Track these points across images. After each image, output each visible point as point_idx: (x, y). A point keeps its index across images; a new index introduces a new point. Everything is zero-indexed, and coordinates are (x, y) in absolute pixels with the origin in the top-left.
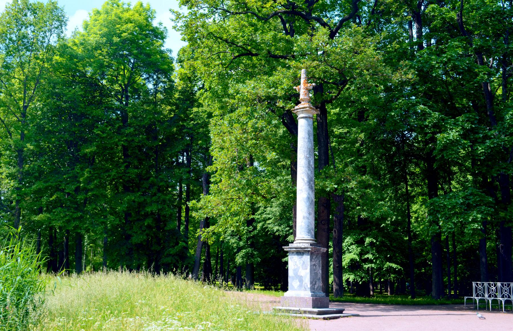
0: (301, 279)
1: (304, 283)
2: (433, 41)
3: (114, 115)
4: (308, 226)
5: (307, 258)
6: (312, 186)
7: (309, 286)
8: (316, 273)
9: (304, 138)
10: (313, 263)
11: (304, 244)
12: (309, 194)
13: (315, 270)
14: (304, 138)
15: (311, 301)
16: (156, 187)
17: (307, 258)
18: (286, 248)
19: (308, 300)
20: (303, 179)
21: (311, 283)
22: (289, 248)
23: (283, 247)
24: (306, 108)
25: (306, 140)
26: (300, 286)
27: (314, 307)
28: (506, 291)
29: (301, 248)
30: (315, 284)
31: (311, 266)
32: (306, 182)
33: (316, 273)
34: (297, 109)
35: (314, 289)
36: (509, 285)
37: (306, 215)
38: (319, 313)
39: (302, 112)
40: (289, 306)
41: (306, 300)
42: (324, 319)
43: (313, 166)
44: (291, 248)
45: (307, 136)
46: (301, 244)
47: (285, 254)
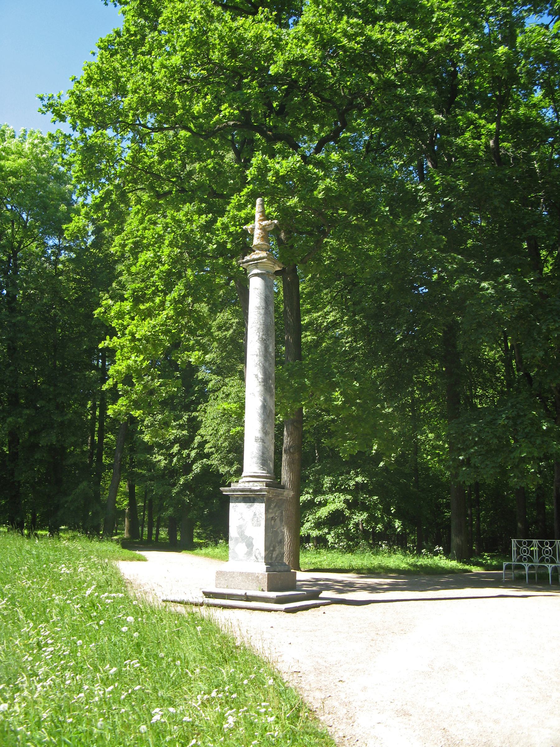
0: (250, 545)
1: (254, 549)
2: (282, 235)
3: (417, 396)
4: (263, 453)
5: (260, 508)
6: (270, 387)
7: (263, 554)
8: (276, 531)
9: (258, 308)
10: (271, 516)
11: (256, 484)
12: (265, 400)
13: (273, 527)
14: (258, 308)
15: (266, 580)
16: (272, 172)
17: (260, 508)
18: (225, 490)
19: (261, 577)
20: (256, 376)
21: (267, 548)
22: (230, 491)
23: (222, 489)
24: (263, 258)
25: (262, 311)
26: (249, 553)
27: (270, 590)
28: (547, 552)
29: (251, 491)
30: (274, 550)
31: (266, 520)
32: (260, 380)
33: (276, 531)
34: (247, 262)
35: (271, 558)
36: (552, 544)
37: (259, 434)
38: (279, 601)
39: (256, 266)
40: (227, 587)
41: (258, 577)
42: (288, 611)
43: (273, 354)
44: (234, 491)
45: (263, 304)
46: (251, 484)
47: (225, 501)
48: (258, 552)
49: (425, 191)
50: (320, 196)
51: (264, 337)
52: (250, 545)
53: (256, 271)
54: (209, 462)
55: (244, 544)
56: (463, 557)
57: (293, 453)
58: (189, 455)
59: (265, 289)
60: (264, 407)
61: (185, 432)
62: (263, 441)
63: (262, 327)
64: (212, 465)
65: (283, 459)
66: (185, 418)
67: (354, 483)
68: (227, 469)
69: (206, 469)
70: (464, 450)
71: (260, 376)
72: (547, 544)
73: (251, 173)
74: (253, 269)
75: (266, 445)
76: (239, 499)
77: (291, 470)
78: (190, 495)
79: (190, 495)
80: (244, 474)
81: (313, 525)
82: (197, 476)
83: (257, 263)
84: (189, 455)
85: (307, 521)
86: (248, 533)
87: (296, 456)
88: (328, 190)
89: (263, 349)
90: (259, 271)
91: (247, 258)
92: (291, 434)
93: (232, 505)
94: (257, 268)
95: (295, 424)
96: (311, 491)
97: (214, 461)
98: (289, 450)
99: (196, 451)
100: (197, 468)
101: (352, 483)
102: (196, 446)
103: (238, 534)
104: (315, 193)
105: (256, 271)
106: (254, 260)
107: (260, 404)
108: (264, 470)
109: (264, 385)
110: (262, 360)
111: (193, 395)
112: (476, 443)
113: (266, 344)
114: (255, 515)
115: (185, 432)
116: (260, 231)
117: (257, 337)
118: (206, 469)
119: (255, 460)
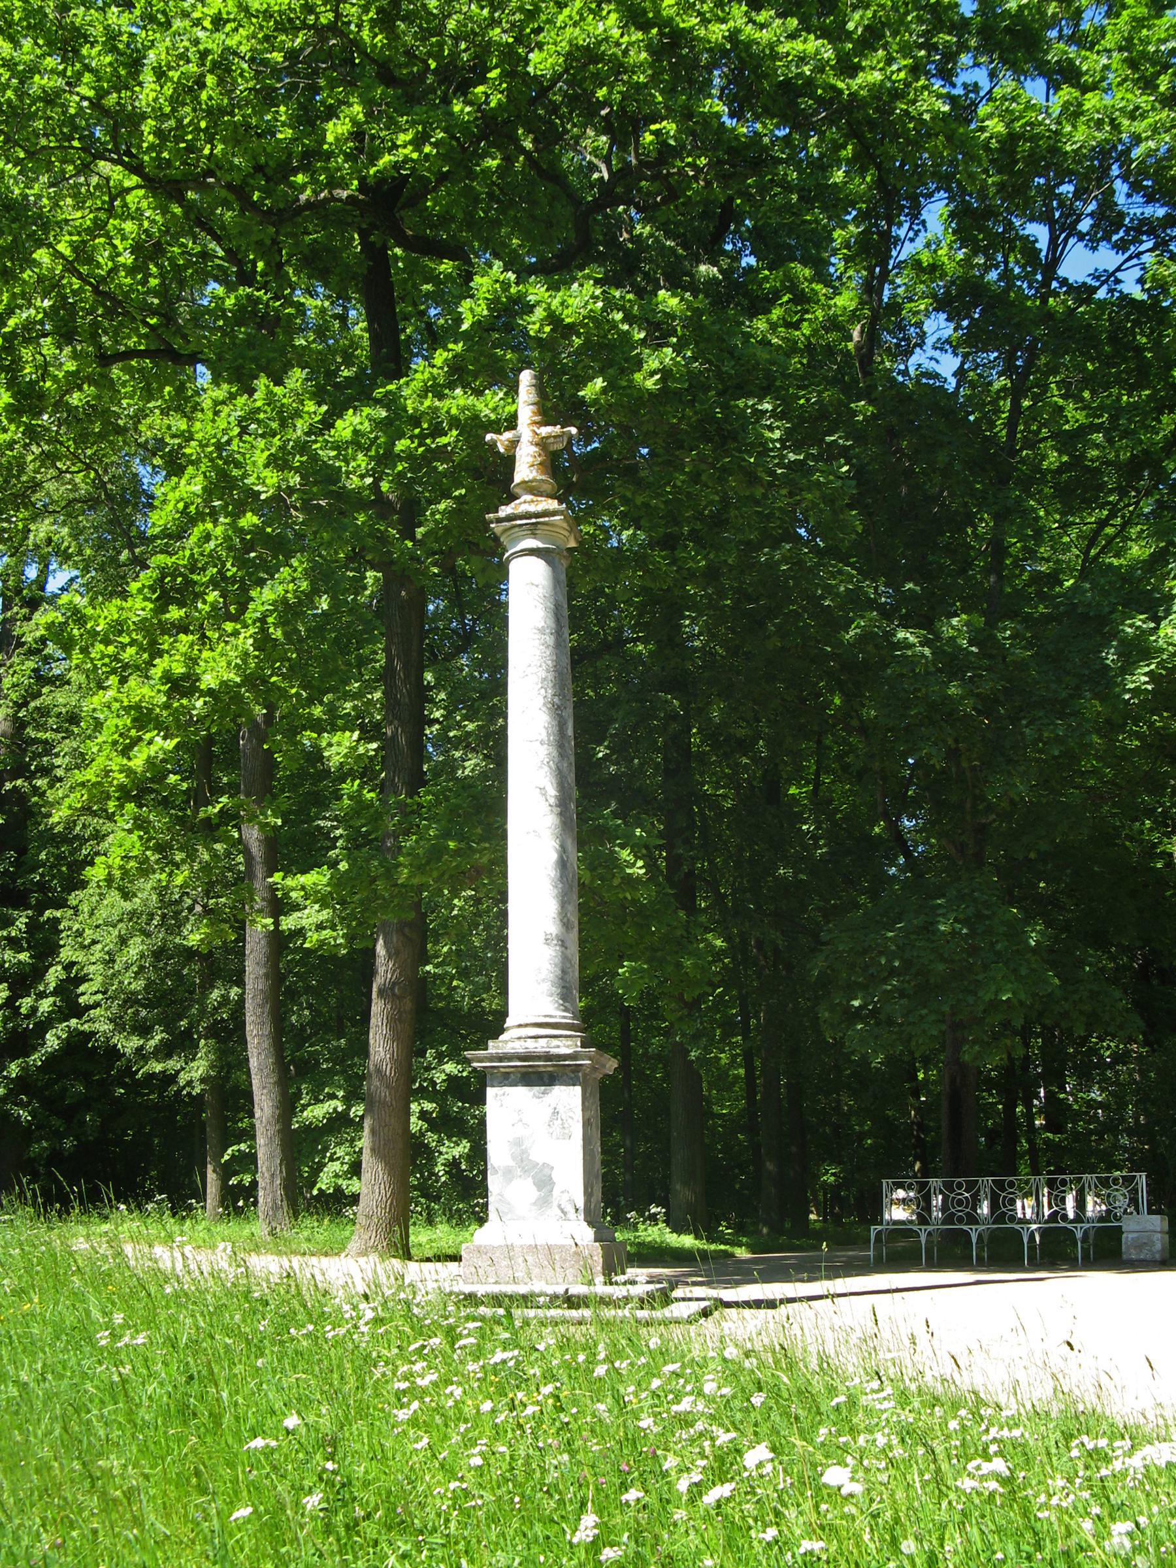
0: (545, 1182)
1: (556, 1192)
7: (581, 1203)
9: (541, 631)
12: (563, 849)
20: (542, 790)
24: (554, 513)
25: (550, 640)
28: (960, 1203)
29: (548, 1057)
32: (552, 801)
39: (533, 530)
45: (551, 622)
46: (543, 1042)
48: (566, 1197)
49: (774, 414)
50: (650, 384)
51: (556, 700)
52: (545, 1182)
53: (531, 543)
54: (86, 1027)
55: (530, 1180)
56: (705, 1227)
57: (400, 998)
58: (34, 1009)
59: (555, 587)
60: (562, 864)
61: (24, 956)
62: (563, 943)
63: (550, 676)
64: (93, 1034)
65: (374, 1009)
66: (22, 922)
67: (443, 1077)
68: (136, 1042)
69: (77, 1043)
70: (864, 987)
71: (552, 792)
72: (960, 1186)
73: (471, 311)
74: (524, 537)
75: (568, 952)
76: (507, 1079)
77: (396, 1035)
78: (29, 1103)
79: (29, 1103)
80: (509, 1022)
81: (346, 1167)
82: (52, 1060)
83: (534, 523)
84: (34, 1009)
85: (332, 1159)
86: (538, 1155)
87: (408, 1004)
88: (666, 374)
89: (556, 729)
90: (541, 545)
91: (505, 511)
92: (397, 953)
93: (491, 1092)
94: (534, 535)
95: (406, 930)
96: (341, 1094)
97: (100, 1024)
98: (392, 989)
99: (51, 999)
100: (52, 1041)
101: (439, 1077)
102: (51, 988)
103: (514, 1158)
104: (638, 377)
105: (531, 543)
106: (528, 516)
107: (554, 856)
108: (566, 1010)
109: (561, 814)
110: (555, 753)
111: (34, 870)
112: (893, 972)
113: (560, 716)
114: (556, 1112)
115: (24, 956)
116: (534, 449)
117: (541, 701)
118: (77, 1043)
119: (547, 987)
